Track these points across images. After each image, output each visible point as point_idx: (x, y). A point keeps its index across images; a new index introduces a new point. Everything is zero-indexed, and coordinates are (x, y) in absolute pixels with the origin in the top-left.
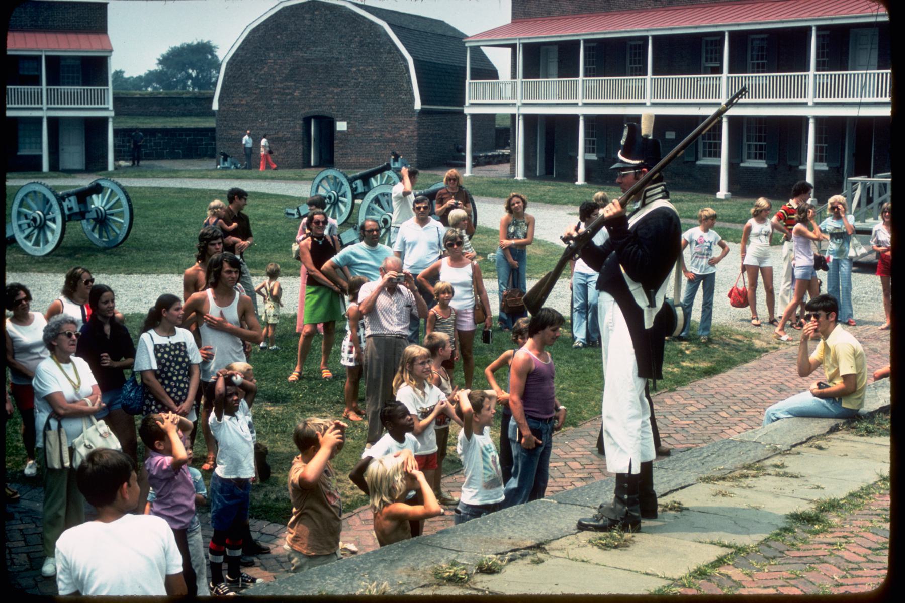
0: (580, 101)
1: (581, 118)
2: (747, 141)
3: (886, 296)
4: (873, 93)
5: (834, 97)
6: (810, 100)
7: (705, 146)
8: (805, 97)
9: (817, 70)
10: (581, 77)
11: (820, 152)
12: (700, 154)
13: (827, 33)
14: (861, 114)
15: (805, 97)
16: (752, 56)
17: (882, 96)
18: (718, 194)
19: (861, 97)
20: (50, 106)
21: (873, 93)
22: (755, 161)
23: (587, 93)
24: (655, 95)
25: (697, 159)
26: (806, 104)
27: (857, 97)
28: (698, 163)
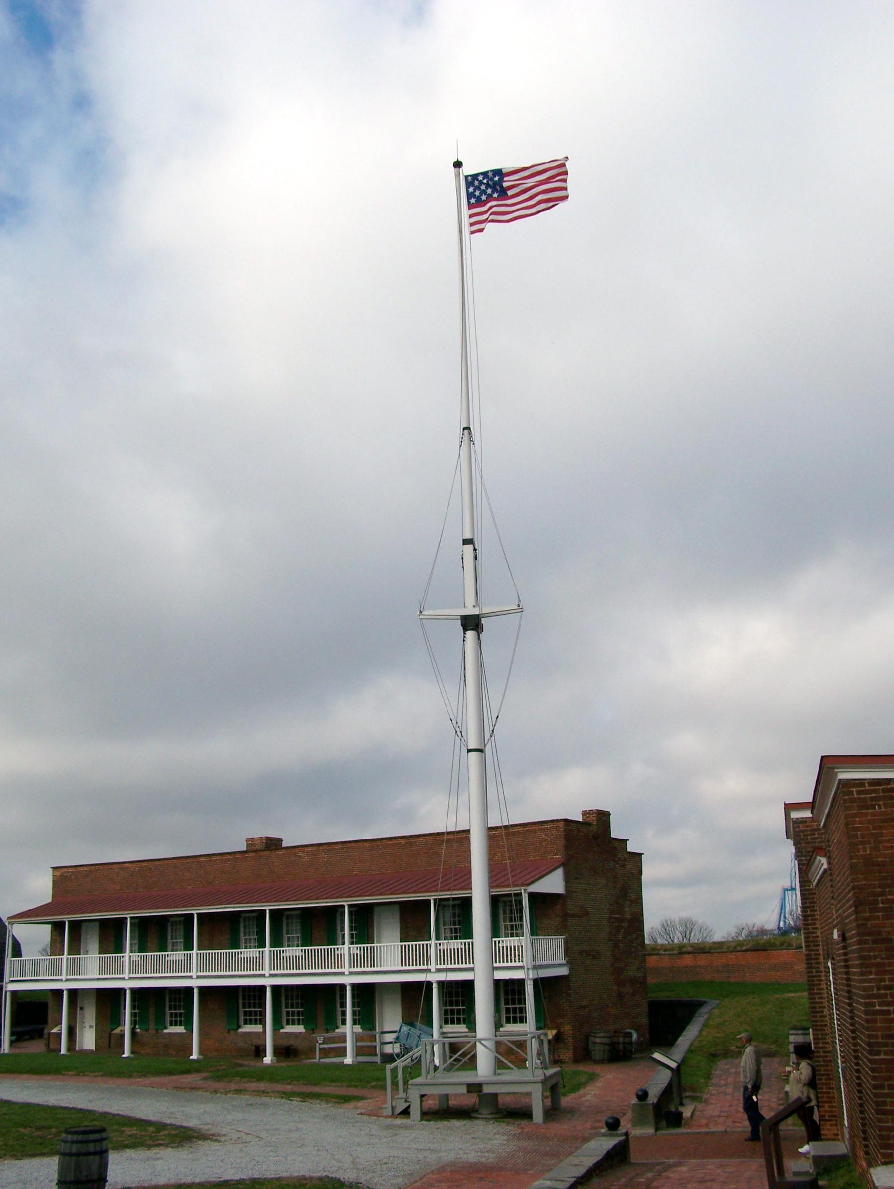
0: (346, 970)
1: (65, 993)
2: (243, 1008)
3: (629, 1156)
4: (455, 960)
5: (371, 966)
6: (432, 967)
7: (171, 1016)
8: (190, 972)
9: (199, 949)
10: (127, 954)
11: (523, 1017)
12: (242, 1022)
13: (459, 902)
14: (448, 979)
15: (262, 970)
16: (444, 922)
17: (306, 969)
18: (264, 1059)
19: (448, 964)
20: (352, 970)
21: (283, 967)
22: (293, 1026)
23: (443, 957)
24: (199, 969)
25: (239, 1027)
26: (191, 977)
27: (424, 964)
28: (241, 1030)
